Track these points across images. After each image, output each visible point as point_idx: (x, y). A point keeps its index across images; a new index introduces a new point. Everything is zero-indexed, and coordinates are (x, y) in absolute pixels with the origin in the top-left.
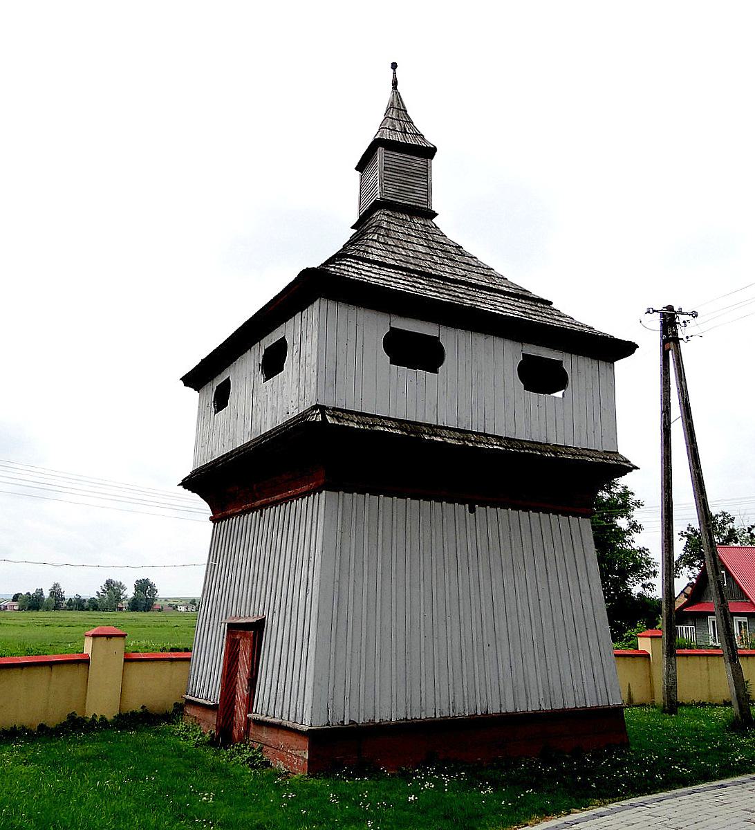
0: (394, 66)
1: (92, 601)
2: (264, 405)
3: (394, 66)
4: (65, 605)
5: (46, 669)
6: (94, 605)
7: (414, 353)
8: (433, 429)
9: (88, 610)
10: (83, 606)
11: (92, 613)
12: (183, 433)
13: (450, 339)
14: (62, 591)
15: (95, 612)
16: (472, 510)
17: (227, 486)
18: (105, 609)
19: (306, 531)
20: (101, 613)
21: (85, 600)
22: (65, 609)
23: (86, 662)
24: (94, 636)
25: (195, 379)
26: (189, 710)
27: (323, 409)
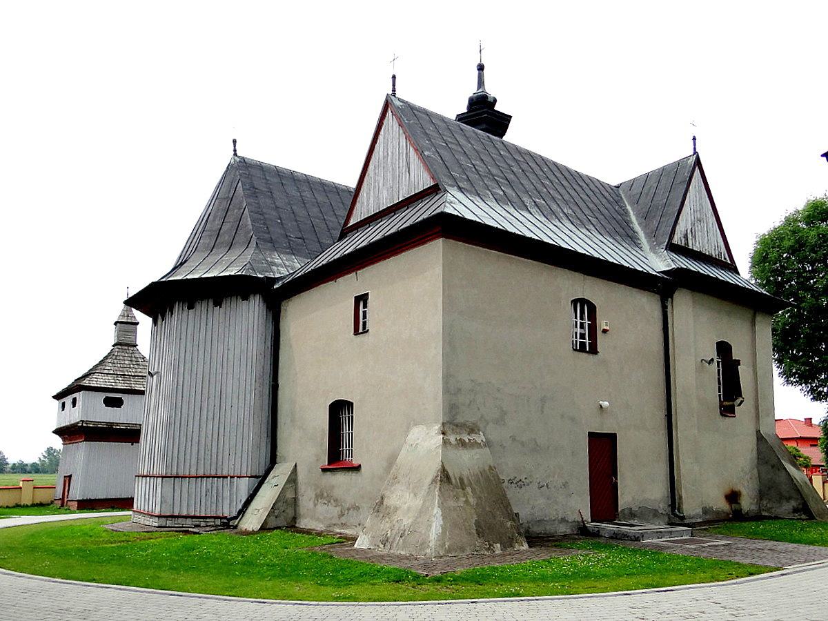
0: (235, 141)
1: (34, 465)
2: (74, 416)
3: (235, 141)
4: (8, 469)
5: (8, 490)
6: (36, 469)
7: (110, 403)
8: (117, 424)
9: (30, 472)
10: (25, 470)
11: (34, 475)
12: (54, 416)
13: (125, 397)
14: (6, 457)
15: (37, 475)
16: (132, 445)
17: (68, 433)
18: (46, 472)
19: (82, 448)
20: (42, 475)
21: (27, 465)
22: (9, 472)
23: (21, 488)
24: (23, 481)
25: (58, 397)
26: (56, 502)
27: (83, 421)
